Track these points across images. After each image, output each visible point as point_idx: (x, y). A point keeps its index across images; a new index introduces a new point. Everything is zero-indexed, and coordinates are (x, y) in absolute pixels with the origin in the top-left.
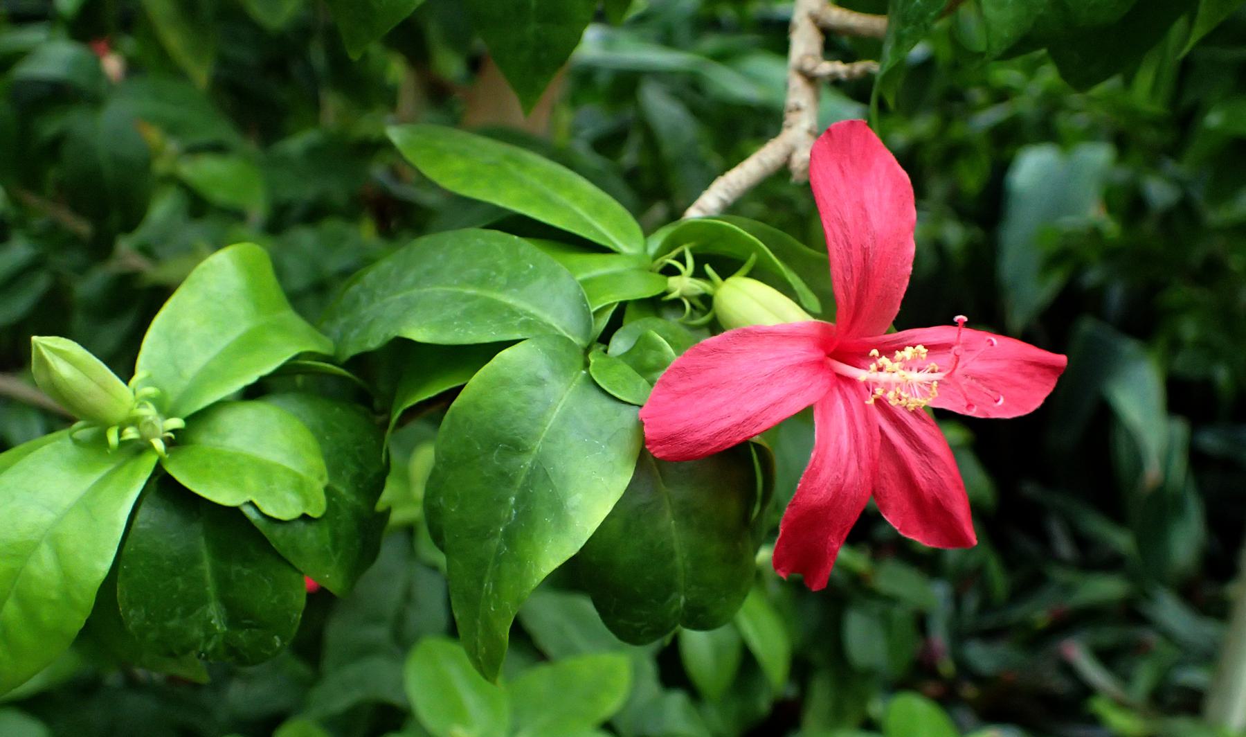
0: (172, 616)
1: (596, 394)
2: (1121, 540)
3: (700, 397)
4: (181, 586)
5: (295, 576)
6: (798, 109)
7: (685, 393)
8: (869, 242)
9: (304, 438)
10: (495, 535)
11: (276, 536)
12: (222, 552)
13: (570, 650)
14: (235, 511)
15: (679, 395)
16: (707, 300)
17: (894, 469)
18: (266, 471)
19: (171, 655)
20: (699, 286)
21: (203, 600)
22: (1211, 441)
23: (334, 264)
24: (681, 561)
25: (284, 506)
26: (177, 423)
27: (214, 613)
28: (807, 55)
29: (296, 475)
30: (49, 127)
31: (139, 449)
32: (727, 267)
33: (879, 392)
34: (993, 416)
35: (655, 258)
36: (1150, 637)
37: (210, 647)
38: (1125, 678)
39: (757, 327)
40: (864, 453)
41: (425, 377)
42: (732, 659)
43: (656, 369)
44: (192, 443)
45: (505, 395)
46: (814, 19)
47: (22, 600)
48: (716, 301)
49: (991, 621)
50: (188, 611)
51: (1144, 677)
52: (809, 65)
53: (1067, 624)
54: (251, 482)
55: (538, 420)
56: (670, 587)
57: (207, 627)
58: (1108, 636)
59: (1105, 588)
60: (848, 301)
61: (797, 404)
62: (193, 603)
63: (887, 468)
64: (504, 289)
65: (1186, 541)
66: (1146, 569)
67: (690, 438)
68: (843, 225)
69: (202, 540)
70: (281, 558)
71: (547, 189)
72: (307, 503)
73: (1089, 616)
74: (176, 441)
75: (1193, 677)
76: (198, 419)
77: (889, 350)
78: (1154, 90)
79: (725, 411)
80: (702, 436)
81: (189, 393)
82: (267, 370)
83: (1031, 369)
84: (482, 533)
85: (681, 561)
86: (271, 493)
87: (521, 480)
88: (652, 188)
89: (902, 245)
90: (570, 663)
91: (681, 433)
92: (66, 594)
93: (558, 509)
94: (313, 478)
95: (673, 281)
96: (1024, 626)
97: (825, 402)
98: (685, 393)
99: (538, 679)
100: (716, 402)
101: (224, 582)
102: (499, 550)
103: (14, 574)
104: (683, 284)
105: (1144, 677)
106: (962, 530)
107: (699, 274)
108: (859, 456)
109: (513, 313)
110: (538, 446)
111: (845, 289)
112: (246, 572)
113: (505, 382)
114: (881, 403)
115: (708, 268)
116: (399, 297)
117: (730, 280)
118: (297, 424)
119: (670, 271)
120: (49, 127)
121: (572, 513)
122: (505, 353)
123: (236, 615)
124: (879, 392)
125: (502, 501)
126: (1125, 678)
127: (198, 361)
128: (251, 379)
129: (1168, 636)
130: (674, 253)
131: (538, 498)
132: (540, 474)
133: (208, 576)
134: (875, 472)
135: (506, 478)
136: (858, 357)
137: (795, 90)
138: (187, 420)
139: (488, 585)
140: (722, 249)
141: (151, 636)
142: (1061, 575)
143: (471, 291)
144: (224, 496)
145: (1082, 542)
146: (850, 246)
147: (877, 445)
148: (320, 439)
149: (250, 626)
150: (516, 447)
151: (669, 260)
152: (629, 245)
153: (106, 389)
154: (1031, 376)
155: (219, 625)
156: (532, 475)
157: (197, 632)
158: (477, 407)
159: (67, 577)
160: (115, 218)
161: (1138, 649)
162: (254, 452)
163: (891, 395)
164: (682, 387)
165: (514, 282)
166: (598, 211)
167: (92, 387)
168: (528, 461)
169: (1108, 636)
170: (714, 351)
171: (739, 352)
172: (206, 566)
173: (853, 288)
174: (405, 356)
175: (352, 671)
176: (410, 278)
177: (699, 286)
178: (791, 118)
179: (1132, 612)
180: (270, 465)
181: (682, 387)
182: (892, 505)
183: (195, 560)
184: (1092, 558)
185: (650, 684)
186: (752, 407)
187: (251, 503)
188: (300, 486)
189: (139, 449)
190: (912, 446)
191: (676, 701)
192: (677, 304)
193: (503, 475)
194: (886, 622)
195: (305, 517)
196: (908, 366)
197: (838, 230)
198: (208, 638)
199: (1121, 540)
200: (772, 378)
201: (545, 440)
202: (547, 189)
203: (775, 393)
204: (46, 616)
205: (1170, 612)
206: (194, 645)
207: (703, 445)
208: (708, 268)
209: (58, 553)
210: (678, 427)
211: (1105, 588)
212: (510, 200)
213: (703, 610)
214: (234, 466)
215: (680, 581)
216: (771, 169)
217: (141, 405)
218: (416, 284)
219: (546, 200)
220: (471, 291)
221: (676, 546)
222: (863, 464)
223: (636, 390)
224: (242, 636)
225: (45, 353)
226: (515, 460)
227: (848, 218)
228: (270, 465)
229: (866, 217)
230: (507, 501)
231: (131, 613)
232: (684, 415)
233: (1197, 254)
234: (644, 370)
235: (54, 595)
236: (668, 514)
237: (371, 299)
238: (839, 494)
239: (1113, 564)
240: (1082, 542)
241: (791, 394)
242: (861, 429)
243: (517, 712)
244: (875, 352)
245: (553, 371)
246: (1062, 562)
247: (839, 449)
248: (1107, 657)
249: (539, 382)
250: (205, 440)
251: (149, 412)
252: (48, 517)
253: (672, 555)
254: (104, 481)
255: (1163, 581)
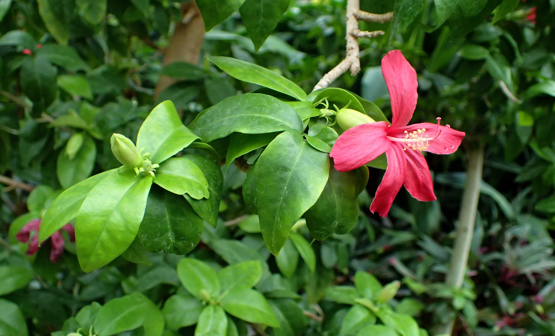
0: (156, 236)
1: (310, 149)
2: (410, 218)
3: (350, 148)
4: (159, 226)
5: (200, 220)
6: (352, 49)
7: (344, 148)
8: (403, 93)
9: (199, 171)
10: (279, 201)
11: (195, 205)
12: (173, 212)
13: (236, 261)
14: (181, 196)
15: (342, 148)
16: (333, 117)
17: (411, 173)
18: (189, 182)
19: (155, 252)
20: (332, 112)
21: (166, 231)
22: (441, 179)
23: (128, 117)
24: (338, 209)
25: (199, 196)
26: (157, 166)
27: (170, 235)
28: (354, 29)
29: (199, 184)
30: (15, 65)
31: (144, 176)
32: (341, 106)
33: (409, 145)
34: (443, 154)
35: (314, 103)
36: (421, 254)
37: (168, 248)
38: (414, 271)
39: (367, 124)
40: (402, 167)
41: (241, 146)
42: (295, 262)
43: (331, 140)
44: (161, 173)
45: (281, 151)
46: (355, 16)
47: (109, 231)
48: (337, 118)
49: (360, 252)
50: (162, 235)
51: (421, 269)
52: (356, 32)
53: (389, 252)
54: (186, 186)
55: (293, 159)
56: (334, 218)
57: (168, 240)
58: (406, 255)
59: (405, 237)
60: (396, 115)
61: (380, 152)
62: (163, 232)
63: (409, 173)
64: (270, 114)
65: (434, 217)
66: (420, 229)
67: (349, 163)
68: (395, 87)
69: (166, 208)
70: (196, 214)
71: (272, 79)
72: (204, 194)
73: (398, 248)
74: (157, 172)
75: (440, 268)
76: (162, 164)
77: (411, 131)
78: (416, 44)
79: (359, 153)
80: (352, 162)
81: (158, 155)
82: (186, 146)
83: (453, 137)
84: (274, 200)
85: (338, 209)
86: (193, 190)
87: (288, 180)
88: (306, 78)
89: (413, 94)
90: (239, 265)
91: (347, 161)
92: (127, 228)
93: (305, 189)
94: (204, 185)
95: (322, 111)
96: (374, 252)
97: (389, 151)
98: (344, 148)
99: (228, 271)
100: (357, 150)
101: (174, 224)
102: (281, 206)
103: (105, 222)
104: (326, 112)
105: (421, 269)
106: (431, 194)
107: (331, 107)
108: (400, 169)
109: (276, 122)
110: (293, 168)
111: (396, 110)
112: (182, 219)
113: (280, 146)
114: (407, 151)
115: (335, 105)
116: (227, 118)
117: (342, 110)
118: (196, 166)
119: (320, 107)
120: (15, 65)
121: (311, 191)
122: (280, 136)
123: (178, 236)
124: (409, 145)
125: (282, 189)
126: (414, 271)
127: (159, 143)
128: (181, 149)
129: (429, 254)
130: (321, 101)
131: (295, 188)
132: (296, 178)
133: (168, 222)
134: (405, 175)
135: (283, 180)
136: (401, 133)
137: (350, 42)
138: (160, 164)
139: (278, 219)
140: (336, 99)
141: (148, 244)
142: (388, 232)
143: (256, 115)
144: (178, 191)
145: (393, 219)
146: (397, 94)
147: (406, 165)
148: (203, 171)
149: (183, 240)
150: (286, 169)
151: (320, 102)
152: (302, 98)
153: (135, 153)
154: (453, 139)
155: (172, 239)
156: (292, 179)
157: (164, 243)
158: (271, 155)
159: (127, 223)
160: (43, 100)
161: (419, 259)
162: (184, 176)
163: (414, 146)
164: (343, 145)
165: (272, 112)
166: (290, 87)
167: (132, 152)
168: (290, 174)
169: (406, 255)
170: (353, 132)
171: (362, 133)
172: (167, 218)
173: (398, 110)
174: (235, 140)
175: (151, 273)
176: (229, 111)
177: (332, 112)
178: (349, 52)
179: (415, 246)
180: (188, 179)
181: (343, 145)
182: (410, 186)
183: (164, 216)
184: (398, 225)
185: (268, 273)
186: (369, 151)
187: (187, 194)
188: (201, 188)
189: (144, 176)
190: (417, 165)
191: (277, 277)
192: (324, 119)
193: (282, 179)
194: (337, 248)
195: (204, 199)
196: (419, 135)
197: (393, 88)
198: (168, 245)
199: (410, 218)
200: (373, 142)
201: (296, 166)
202: (272, 79)
203: (375, 147)
204: (119, 237)
205: (430, 245)
206: (163, 248)
207: (353, 165)
208: (335, 105)
209: (121, 214)
210: (344, 160)
211: (405, 237)
212: (261, 83)
213: (343, 227)
214: (178, 181)
215: (337, 216)
216: (344, 71)
217: (145, 160)
218: (232, 112)
219: (274, 83)
220: (256, 115)
221: (337, 204)
222: (402, 172)
223: (324, 147)
224: (180, 244)
225: (118, 140)
226: (285, 174)
227: (397, 85)
228: (188, 179)
229: (402, 83)
230: (283, 188)
231: (142, 236)
232: (346, 155)
233: (440, 106)
234: (326, 141)
235: (122, 229)
236: (334, 192)
237: (212, 120)
238: (395, 182)
239: (407, 227)
240: (393, 219)
241: (380, 147)
242: (401, 160)
243: (222, 284)
244: (406, 132)
245: (295, 141)
246: (387, 227)
247: (395, 167)
248: (406, 263)
249: (292, 146)
250: (164, 171)
251: (148, 162)
252: (115, 202)
253: (335, 206)
254: (133, 188)
255: (426, 233)
